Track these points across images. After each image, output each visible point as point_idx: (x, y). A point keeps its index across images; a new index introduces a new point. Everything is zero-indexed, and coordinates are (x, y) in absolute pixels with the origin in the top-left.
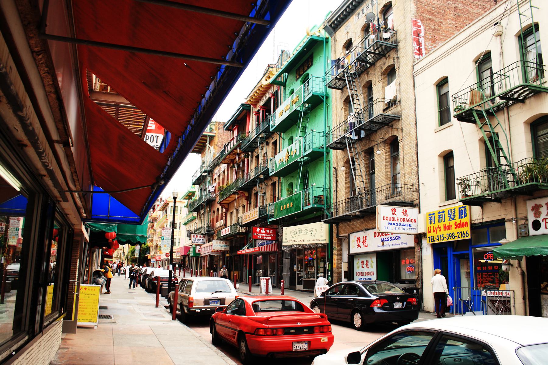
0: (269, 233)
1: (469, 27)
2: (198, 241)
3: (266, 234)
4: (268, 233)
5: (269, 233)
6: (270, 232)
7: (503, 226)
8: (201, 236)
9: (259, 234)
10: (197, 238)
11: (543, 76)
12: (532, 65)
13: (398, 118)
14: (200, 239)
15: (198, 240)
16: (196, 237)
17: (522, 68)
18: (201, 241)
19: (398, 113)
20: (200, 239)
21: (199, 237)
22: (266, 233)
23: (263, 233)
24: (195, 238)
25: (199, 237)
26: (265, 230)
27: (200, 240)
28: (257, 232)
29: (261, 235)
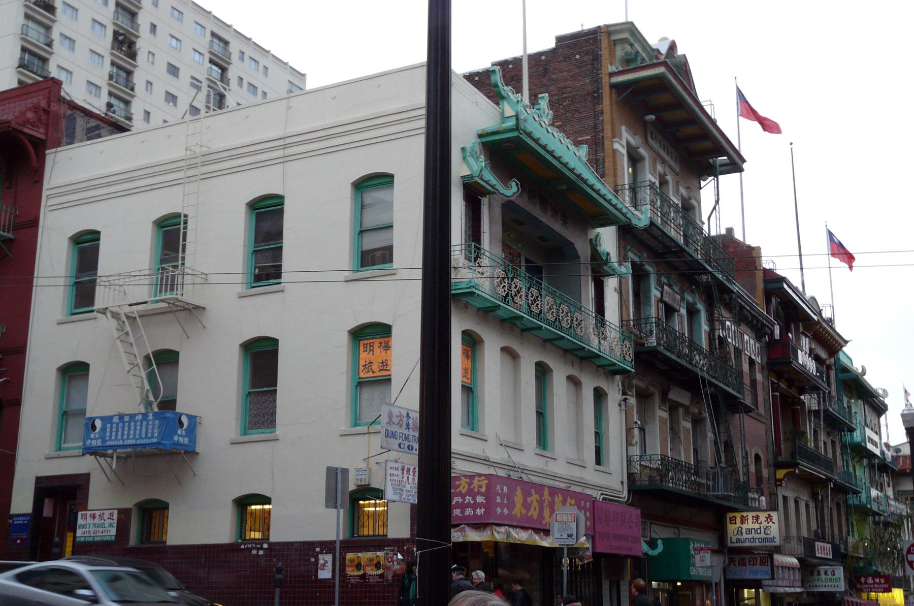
0: (880, 583)
1: (887, 425)
2: (750, 536)
3: (876, 585)
4: (877, 584)
5: (880, 583)
6: (880, 581)
7: (908, 426)
8: (757, 517)
9: (865, 586)
10: (745, 526)
11: (6, 123)
12: (747, 388)
13: (388, 377)
14: (756, 526)
15: (749, 531)
16: (742, 523)
17: (64, 290)
18: (763, 535)
19: (538, 449)
20: (756, 526)
21: (750, 520)
22: (874, 583)
23: (870, 584)
24: (739, 524)
25: (750, 520)
26: (873, 579)
27: (756, 530)
28: (861, 583)
29: (867, 586)
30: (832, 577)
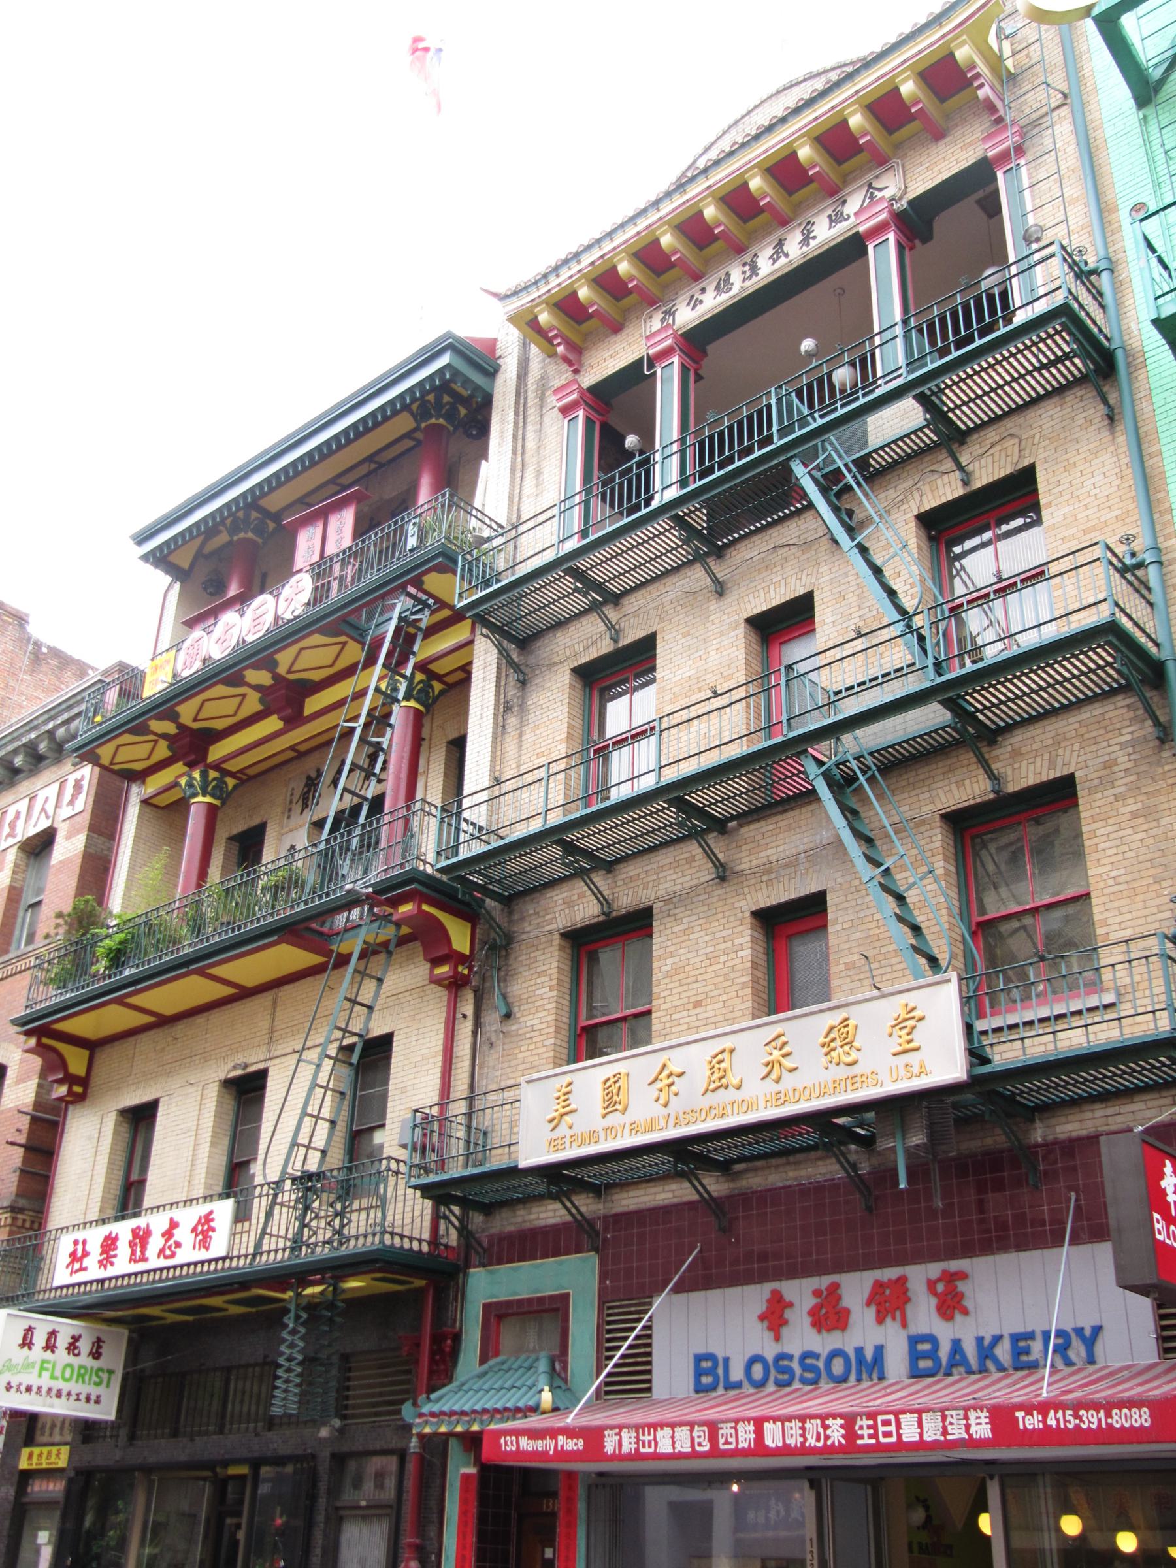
30: (822, 1343)
